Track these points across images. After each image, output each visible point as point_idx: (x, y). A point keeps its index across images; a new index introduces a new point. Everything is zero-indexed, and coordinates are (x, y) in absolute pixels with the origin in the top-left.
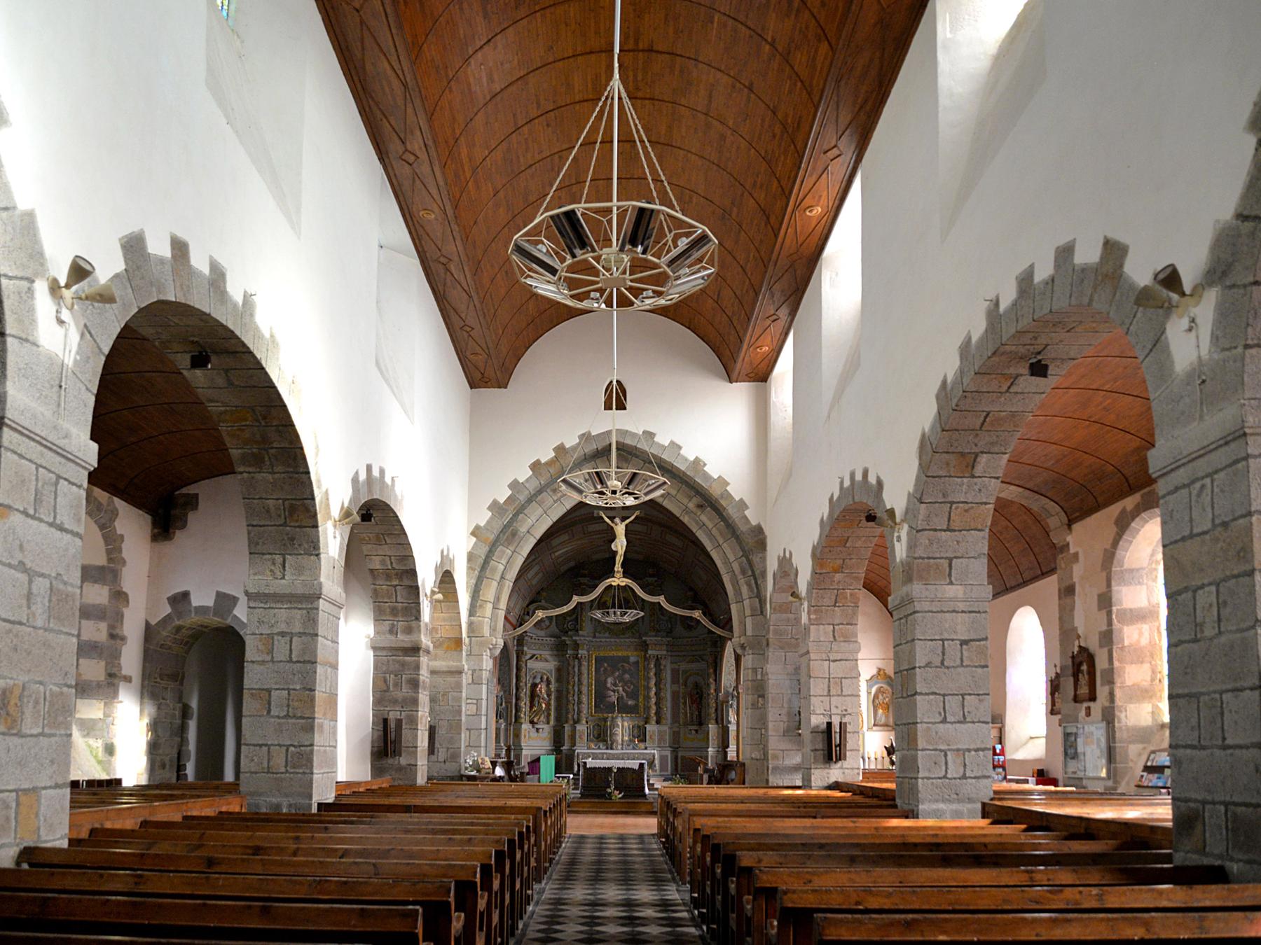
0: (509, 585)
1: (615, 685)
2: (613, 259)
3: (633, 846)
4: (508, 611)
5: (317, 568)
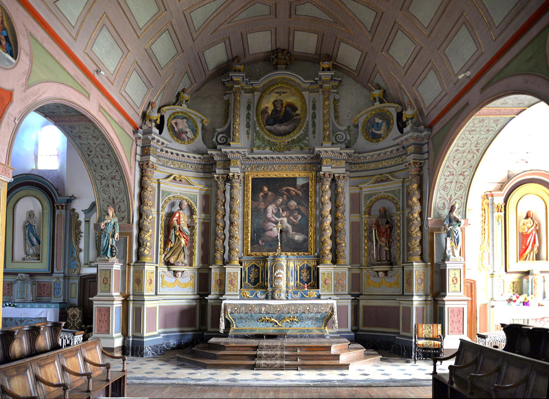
1: (278, 215)
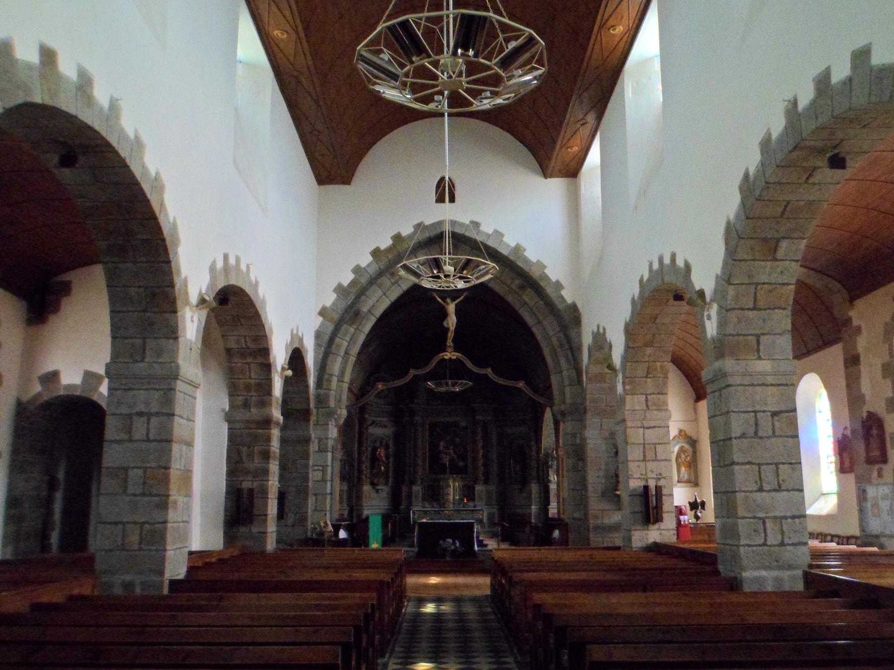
0: (352, 359)
1: (447, 448)
2: (450, 64)
3: (469, 609)
4: (351, 383)
5: (175, 352)
